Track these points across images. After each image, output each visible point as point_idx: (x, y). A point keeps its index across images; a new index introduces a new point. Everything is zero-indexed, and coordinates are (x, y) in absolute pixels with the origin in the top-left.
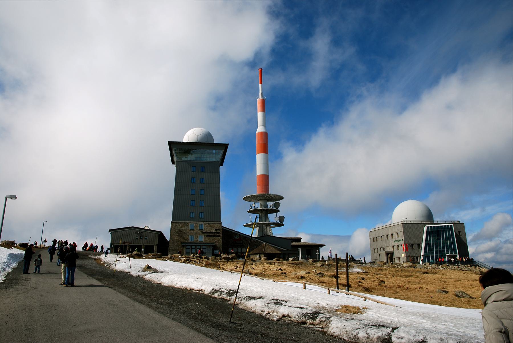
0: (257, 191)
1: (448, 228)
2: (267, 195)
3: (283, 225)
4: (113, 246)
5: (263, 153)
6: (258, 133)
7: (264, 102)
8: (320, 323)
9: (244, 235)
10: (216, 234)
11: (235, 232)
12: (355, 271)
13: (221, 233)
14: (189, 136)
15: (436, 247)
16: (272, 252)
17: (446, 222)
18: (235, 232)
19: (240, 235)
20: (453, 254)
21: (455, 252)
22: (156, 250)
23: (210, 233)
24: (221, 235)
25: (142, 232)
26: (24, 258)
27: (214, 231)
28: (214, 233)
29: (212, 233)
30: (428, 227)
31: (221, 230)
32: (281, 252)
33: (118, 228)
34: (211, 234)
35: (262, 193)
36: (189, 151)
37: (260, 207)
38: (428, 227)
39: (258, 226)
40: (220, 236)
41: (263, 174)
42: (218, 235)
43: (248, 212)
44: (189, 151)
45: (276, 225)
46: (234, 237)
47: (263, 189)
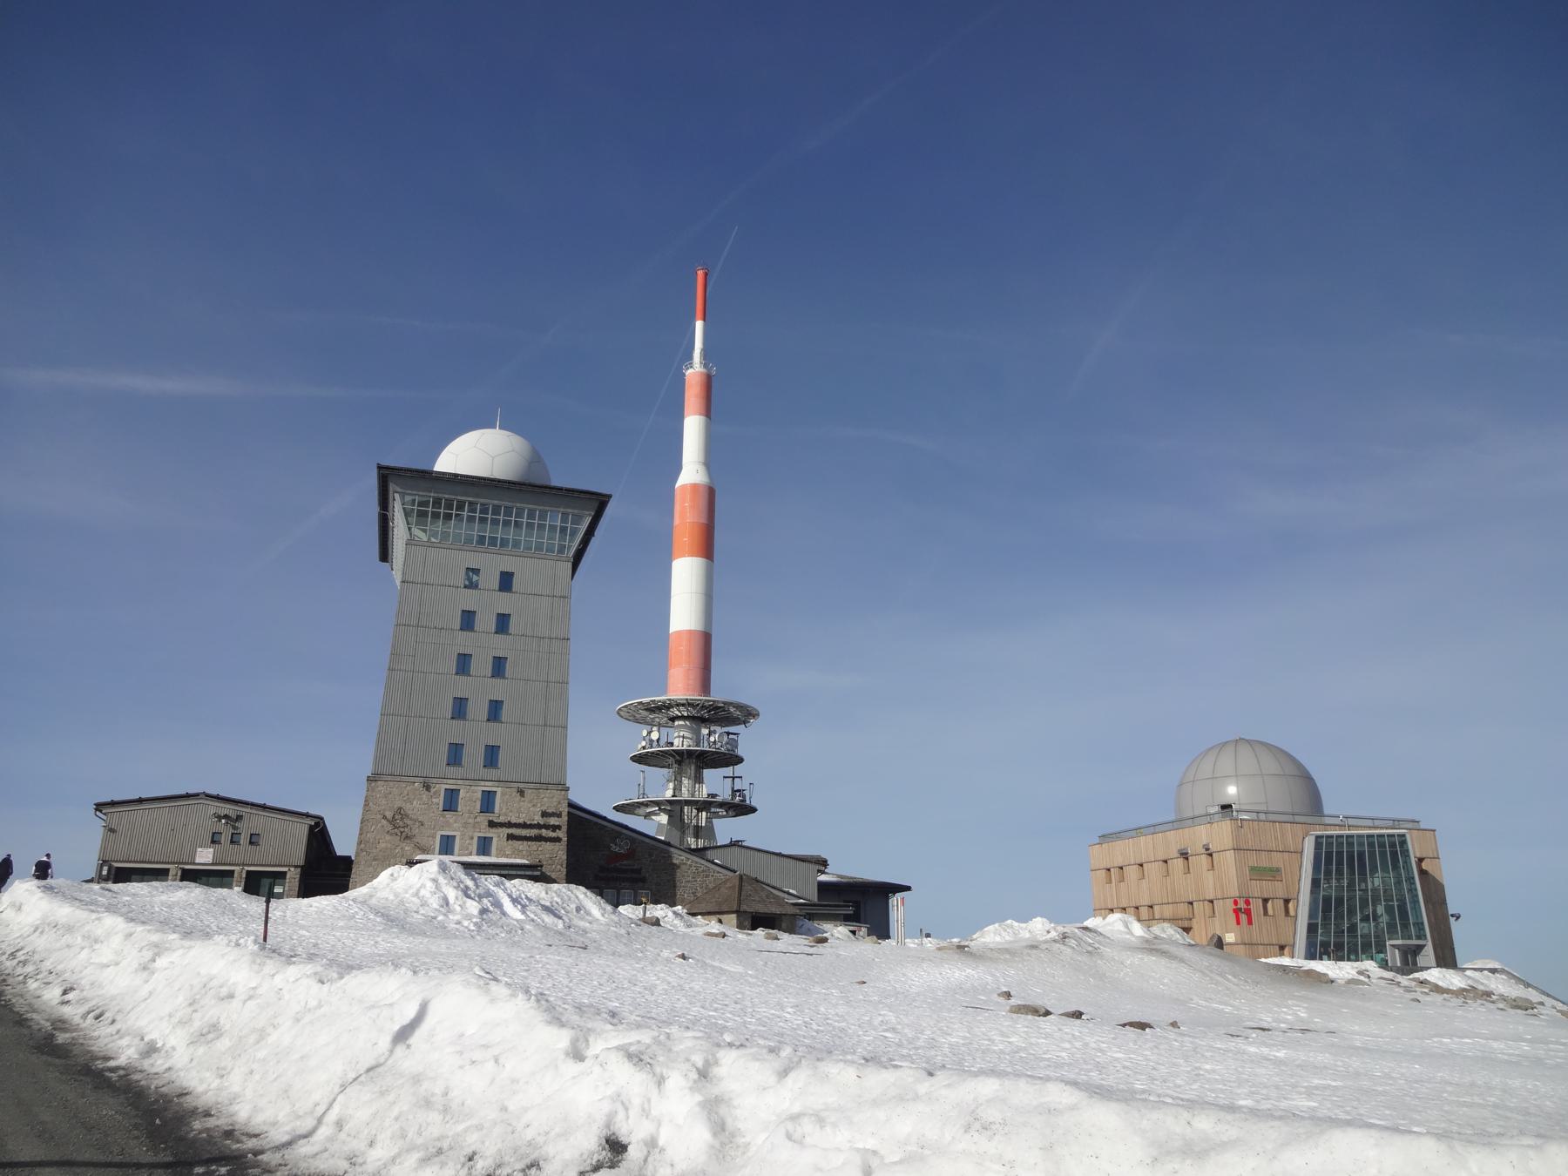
0: (679, 686)
2: (706, 700)
3: (753, 810)
4: (109, 871)
6: (683, 487)
7: (708, 383)
9: (647, 840)
10: (544, 832)
11: (613, 826)
13: (565, 828)
14: (493, 458)
16: (766, 910)
17: (1377, 823)
18: (613, 826)
19: (633, 840)
20: (1415, 942)
21: (1421, 936)
23: (524, 826)
24: (562, 834)
25: (239, 818)
26: (46, 879)
27: (538, 819)
28: (539, 826)
29: (531, 826)
30: (1318, 837)
31: (565, 818)
32: (801, 909)
33: (109, 800)
34: (524, 832)
35: (685, 695)
37: (678, 744)
38: (1318, 837)
39: (665, 811)
40: (558, 840)
41: (693, 628)
42: (553, 835)
45: (729, 808)
46: (609, 847)
47: (691, 682)
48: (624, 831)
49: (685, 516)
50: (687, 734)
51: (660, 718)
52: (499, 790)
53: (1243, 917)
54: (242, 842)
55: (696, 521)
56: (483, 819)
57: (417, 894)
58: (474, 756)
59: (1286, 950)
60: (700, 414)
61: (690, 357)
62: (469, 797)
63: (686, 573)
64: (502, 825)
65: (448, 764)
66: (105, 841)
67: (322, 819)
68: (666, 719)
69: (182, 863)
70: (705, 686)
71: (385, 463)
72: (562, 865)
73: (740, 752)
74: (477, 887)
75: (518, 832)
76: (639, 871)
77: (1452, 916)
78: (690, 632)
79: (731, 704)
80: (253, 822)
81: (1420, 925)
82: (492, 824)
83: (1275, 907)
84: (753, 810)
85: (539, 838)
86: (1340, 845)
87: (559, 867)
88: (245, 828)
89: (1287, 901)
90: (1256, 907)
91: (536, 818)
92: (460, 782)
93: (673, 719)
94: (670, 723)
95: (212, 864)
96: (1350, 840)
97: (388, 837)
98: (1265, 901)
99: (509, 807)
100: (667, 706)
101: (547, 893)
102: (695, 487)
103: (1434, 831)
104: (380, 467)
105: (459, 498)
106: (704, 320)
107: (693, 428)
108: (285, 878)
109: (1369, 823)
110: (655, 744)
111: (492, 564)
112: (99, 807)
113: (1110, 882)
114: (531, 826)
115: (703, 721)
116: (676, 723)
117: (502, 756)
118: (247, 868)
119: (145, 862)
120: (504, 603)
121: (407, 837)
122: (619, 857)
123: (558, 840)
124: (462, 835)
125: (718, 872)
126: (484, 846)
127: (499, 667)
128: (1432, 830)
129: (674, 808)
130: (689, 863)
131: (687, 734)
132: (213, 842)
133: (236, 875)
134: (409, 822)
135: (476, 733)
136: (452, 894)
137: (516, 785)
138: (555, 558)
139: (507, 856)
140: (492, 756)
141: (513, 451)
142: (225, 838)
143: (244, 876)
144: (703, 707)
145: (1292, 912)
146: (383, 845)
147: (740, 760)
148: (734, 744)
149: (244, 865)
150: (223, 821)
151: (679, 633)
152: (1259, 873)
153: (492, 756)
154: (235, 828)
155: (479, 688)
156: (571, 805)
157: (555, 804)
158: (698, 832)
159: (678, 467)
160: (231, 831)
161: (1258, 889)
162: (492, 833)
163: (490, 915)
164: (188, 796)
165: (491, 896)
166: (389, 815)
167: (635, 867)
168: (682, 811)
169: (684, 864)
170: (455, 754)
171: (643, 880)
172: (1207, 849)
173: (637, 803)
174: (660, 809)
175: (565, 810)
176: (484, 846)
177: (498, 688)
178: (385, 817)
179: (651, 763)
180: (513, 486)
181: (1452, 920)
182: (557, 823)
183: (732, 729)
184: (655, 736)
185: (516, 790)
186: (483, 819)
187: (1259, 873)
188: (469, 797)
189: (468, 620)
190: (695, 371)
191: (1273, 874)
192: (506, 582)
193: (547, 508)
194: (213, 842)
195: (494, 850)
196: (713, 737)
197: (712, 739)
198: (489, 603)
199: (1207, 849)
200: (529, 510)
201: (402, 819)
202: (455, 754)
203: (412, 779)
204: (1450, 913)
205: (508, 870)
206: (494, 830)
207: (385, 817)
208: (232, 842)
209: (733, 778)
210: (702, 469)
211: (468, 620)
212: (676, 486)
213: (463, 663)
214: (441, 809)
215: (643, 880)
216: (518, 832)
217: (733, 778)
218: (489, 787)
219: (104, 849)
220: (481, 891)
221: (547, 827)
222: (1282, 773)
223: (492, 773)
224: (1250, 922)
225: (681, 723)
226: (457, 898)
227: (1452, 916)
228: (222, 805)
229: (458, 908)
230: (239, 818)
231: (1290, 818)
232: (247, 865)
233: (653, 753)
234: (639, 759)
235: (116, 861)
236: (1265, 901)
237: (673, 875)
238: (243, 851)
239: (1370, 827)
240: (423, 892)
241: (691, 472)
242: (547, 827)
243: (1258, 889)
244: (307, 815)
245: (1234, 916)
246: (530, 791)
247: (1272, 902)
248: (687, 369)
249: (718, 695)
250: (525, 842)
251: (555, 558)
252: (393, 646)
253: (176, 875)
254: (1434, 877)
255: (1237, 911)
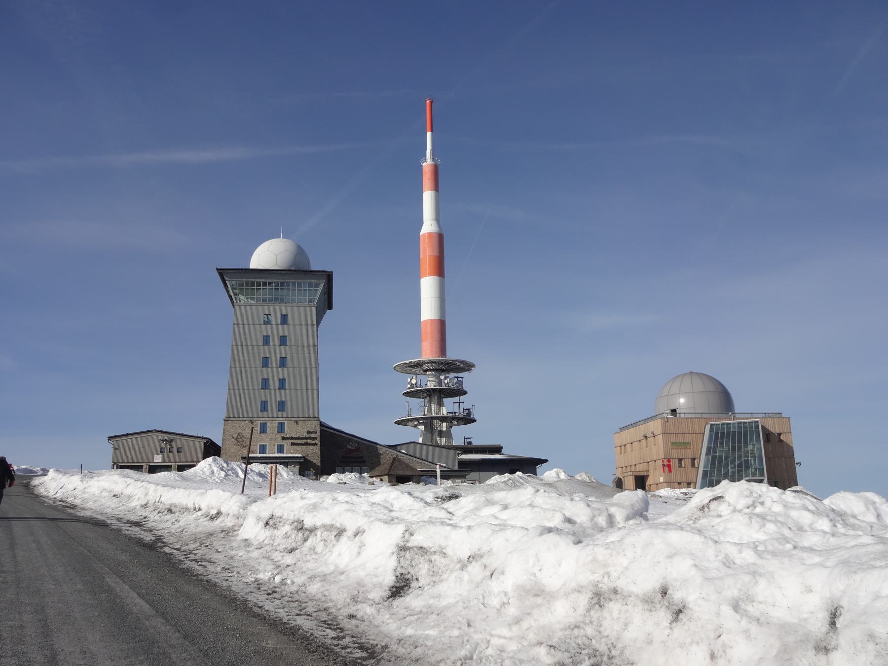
0: (428, 352)
1: (751, 427)
3: (474, 421)
5: (434, 275)
6: (424, 234)
7: (436, 170)
8: (418, 595)
9: (366, 442)
10: (309, 441)
12: (776, 526)
15: (727, 465)
17: (754, 416)
18: (348, 436)
19: (358, 443)
21: (763, 475)
22: (699, 487)
23: (299, 438)
24: (318, 441)
25: (172, 440)
27: (305, 435)
28: (306, 438)
29: (302, 438)
30: (712, 425)
33: (160, 430)
36: (263, 286)
38: (712, 425)
39: (422, 424)
40: (316, 444)
43: (404, 394)
44: (263, 286)
46: (346, 446)
48: (354, 438)
49: (427, 252)
50: (431, 379)
51: (418, 370)
52: (286, 422)
53: (666, 469)
54: (174, 452)
55: (435, 255)
56: (279, 436)
57: (202, 470)
58: (273, 406)
59: (692, 485)
60: (432, 190)
61: (425, 155)
62: (272, 426)
63: (428, 285)
64: (288, 438)
65: (261, 411)
66: (114, 454)
67: (209, 439)
68: (422, 371)
69: (148, 462)
70: (443, 350)
71: (219, 267)
72: (318, 456)
73: (465, 388)
74: (228, 467)
75: (296, 441)
76: (362, 458)
77: (797, 464)
78: (432, 320)
79: (456, 361)
80: (178, 442)
81: (761, 470)
82: (283, 438)
83: (687, 463)
84: (474, 421)
85: (306, 444)
86: (740, 428)
87: (317, 457)
88: (175, 445)
89: (693, 460)
90: (674, 464)
91: (305, 434)
92: (267, 419)
93: (426, 371)
94: (423, 373)
95: (162, 462)
96: (729, 426)
97: (235, 447)
98: (680, 460)
99: (291, 430)
100: (419, 365)
101: (265, 468)
102: (430, 234)
103: (789, 418)
104: (218, 269)
105: (257, 280)
106: (432, 131)
107: (428, 198)
108: (142, 468)
109: (750, 416)
110: (415, 386)
111: (276, 311)
112: (110, 438)
113: (621, 453)
114: (302, 438)
115: (441, 371)
116: (427, 373)
117: (287, 406)
118: (177, 464)
119: (132, 463)
120: (283, 330)
121: (244, 446)
122: (352, 451)
123: (316, 444)
124: (269, 444)
125: (403, 457)
126: (280, 449)
127: (283, 362)
128: (787, 418)
129: (428, 422)
130: (387, 452)
131: (431, 379)
132: (161, 452)
133: (173, 467)
134: (244, 439)
135: (273, 396)
136: (215, 469)
137: (294, 419)
138: (308, 305)
139: (291, 453)
140: (282, 406)
141: (287, 250)
142: (166, 450)
143: (176, 467)
144: (442, 363)
145: (696, 466)
146: (233, 451)
147: (465, 393)
148: (460, 383)
149: (176, 462)
150: (165, 442)
151: (426, 321)
152: (676, 445)
153: (282, 406)
154: (170, 445)
155: (274, 374)
156: (322, 425)
157: (314, 427)
158: (441, 434)
159: (419, 222)
160: (169, 447)
161: (675, 454)
162: (283, 442)
163: (229, 477)
164: (148, 432)
165: (233, 470)
166: (235, 436)
167: (360, 456)
168: (431, 423)
169: (385, 453)
170: (264, 406)
171: (364, 462)
172: (653, 434)
173: (406, 420)
174: (419, 422)
175: (318, 429)
176: (280, 449)
177: (283, 373)
178: (233, 438)
179: (417, 397)
180: (282, 272)
181: (797, 466)
182: (315, 437)
183: (459, 375)
184: (414, 382)
185: (294, 422)
186: (279, 436)
187: (676, 445)
188: (272, 426)
189: (266, 340)
190: (428, 163)
191: (685, 445)
192: (284, 319)
193: (301, 281)
194: (161, 452)
195: (285, 452)
196: (449, 380)
197: (446, 381)
198: (275, 331)
199: (653, 434)
200: (292, 283)
201: (241, 438)
202: (264, 406)
203: (244, 419)
204: (796, 462)
205: (288, 460)
206: (285, 441)
207: (233, 438)
208: (170, 452)
209: (460, 403)
210: (434, 223)
211: (266, 340)
212: (421, 234)
213: (266, 362)
214: (259, 432)
215: (364, 462)
216: (296, 441)
217: (460, 403)
218: (281, 421)
219: (114, 457)
220: (229, 468)
221: (310, 438)
222: (704, 391)
223: (282, 414)
224: (670, 471)
225: (430, 373)
226: (217, 471)
227: (797, 464)
228: (164, 435)
229: (217, 475)
230: (172, 440)
231: (699, 416)
232: (178, 462)
233: (413, 391)
234: (407, 394)
235: (120, 463)
236: (680, 460)
237: (379, 459)
238: (175, 456)
239: (751, 418)
240: (205, 469)
241: (429, 226)
242: (310, 438)
243: (681, 453)
244: (203, 438)
245: (662, 468)
246: (301, 422)
247: (685, 460)
248: (423, 163)
249: (452, 355)
250: (300, 446)
251: (308, 305)
252: (232, 356)
253: (146, 468)
254: (787, 444)
255: (664, 465)
